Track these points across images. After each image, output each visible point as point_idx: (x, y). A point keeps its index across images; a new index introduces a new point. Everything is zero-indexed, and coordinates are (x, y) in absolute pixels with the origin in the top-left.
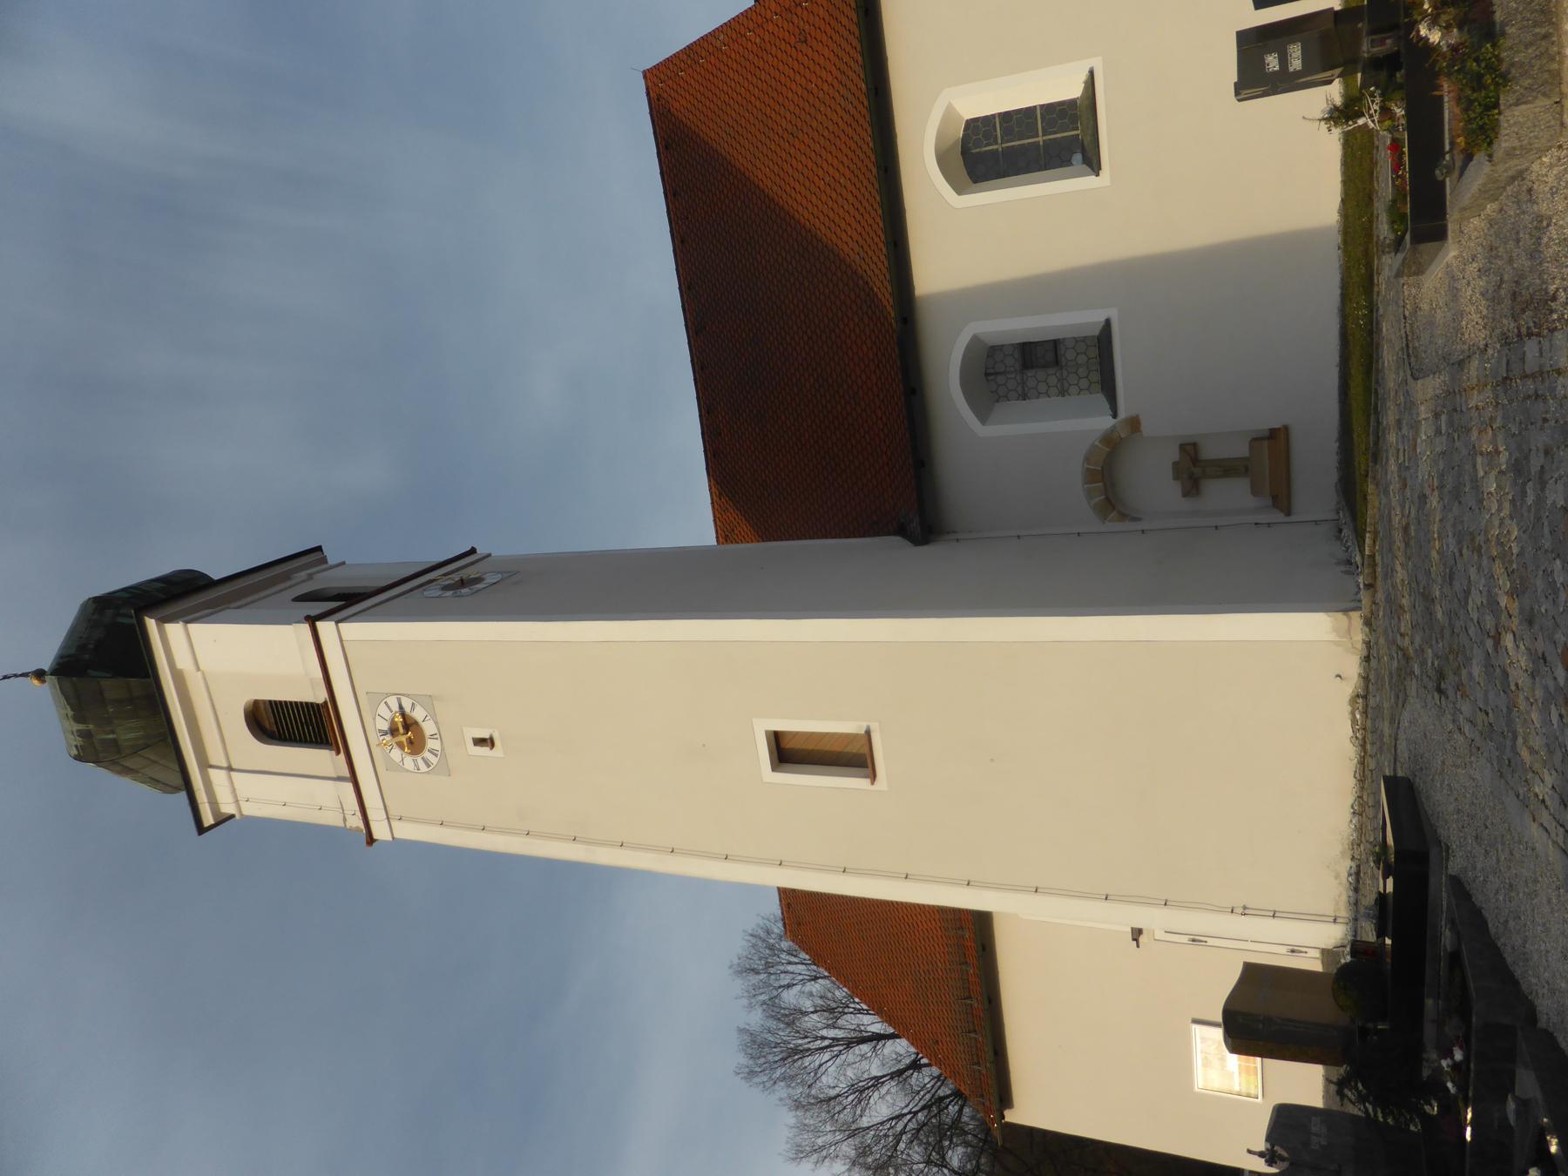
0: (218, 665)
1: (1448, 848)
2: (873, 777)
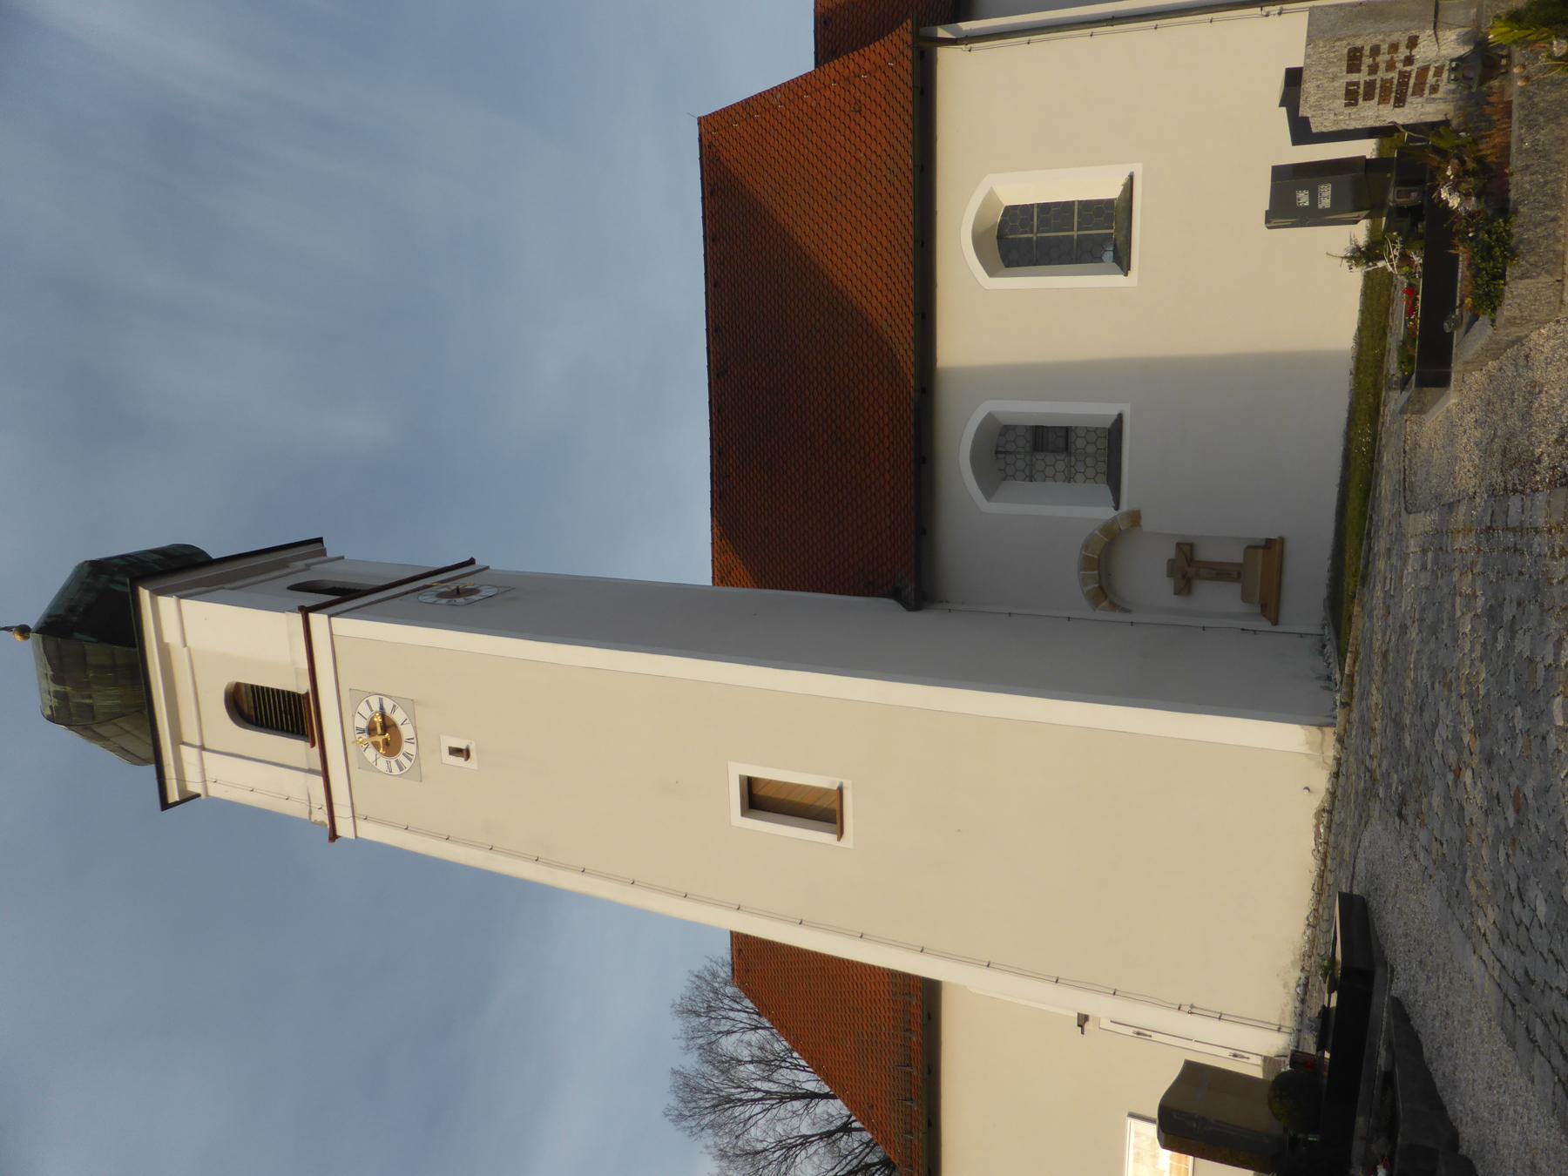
0: (205, 643)
1: (1393, 970)
2: (840, 833)
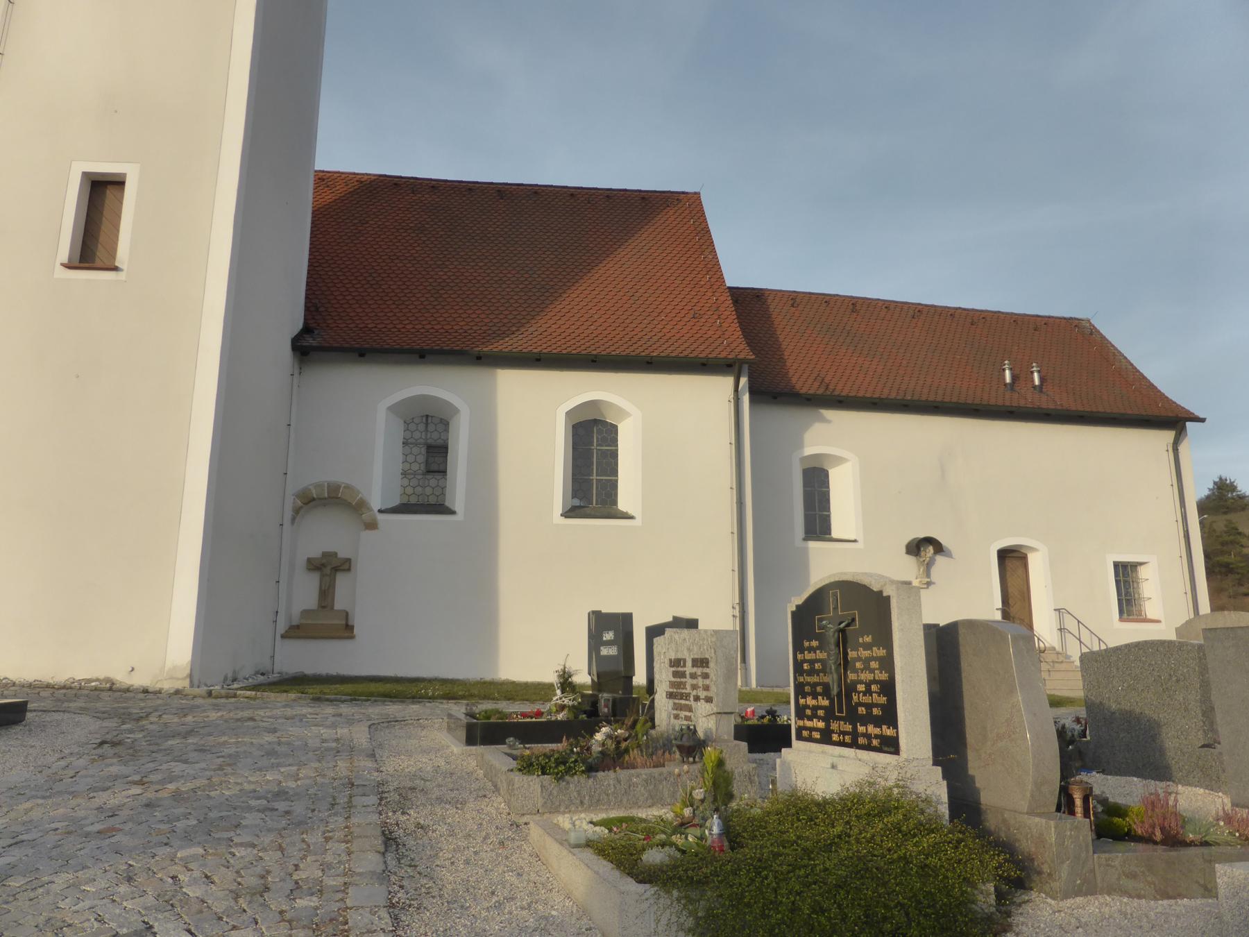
2: (69, 266)
